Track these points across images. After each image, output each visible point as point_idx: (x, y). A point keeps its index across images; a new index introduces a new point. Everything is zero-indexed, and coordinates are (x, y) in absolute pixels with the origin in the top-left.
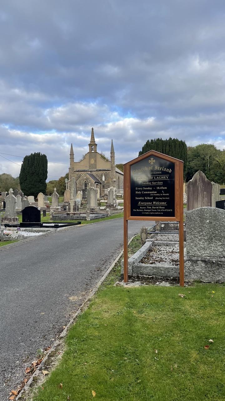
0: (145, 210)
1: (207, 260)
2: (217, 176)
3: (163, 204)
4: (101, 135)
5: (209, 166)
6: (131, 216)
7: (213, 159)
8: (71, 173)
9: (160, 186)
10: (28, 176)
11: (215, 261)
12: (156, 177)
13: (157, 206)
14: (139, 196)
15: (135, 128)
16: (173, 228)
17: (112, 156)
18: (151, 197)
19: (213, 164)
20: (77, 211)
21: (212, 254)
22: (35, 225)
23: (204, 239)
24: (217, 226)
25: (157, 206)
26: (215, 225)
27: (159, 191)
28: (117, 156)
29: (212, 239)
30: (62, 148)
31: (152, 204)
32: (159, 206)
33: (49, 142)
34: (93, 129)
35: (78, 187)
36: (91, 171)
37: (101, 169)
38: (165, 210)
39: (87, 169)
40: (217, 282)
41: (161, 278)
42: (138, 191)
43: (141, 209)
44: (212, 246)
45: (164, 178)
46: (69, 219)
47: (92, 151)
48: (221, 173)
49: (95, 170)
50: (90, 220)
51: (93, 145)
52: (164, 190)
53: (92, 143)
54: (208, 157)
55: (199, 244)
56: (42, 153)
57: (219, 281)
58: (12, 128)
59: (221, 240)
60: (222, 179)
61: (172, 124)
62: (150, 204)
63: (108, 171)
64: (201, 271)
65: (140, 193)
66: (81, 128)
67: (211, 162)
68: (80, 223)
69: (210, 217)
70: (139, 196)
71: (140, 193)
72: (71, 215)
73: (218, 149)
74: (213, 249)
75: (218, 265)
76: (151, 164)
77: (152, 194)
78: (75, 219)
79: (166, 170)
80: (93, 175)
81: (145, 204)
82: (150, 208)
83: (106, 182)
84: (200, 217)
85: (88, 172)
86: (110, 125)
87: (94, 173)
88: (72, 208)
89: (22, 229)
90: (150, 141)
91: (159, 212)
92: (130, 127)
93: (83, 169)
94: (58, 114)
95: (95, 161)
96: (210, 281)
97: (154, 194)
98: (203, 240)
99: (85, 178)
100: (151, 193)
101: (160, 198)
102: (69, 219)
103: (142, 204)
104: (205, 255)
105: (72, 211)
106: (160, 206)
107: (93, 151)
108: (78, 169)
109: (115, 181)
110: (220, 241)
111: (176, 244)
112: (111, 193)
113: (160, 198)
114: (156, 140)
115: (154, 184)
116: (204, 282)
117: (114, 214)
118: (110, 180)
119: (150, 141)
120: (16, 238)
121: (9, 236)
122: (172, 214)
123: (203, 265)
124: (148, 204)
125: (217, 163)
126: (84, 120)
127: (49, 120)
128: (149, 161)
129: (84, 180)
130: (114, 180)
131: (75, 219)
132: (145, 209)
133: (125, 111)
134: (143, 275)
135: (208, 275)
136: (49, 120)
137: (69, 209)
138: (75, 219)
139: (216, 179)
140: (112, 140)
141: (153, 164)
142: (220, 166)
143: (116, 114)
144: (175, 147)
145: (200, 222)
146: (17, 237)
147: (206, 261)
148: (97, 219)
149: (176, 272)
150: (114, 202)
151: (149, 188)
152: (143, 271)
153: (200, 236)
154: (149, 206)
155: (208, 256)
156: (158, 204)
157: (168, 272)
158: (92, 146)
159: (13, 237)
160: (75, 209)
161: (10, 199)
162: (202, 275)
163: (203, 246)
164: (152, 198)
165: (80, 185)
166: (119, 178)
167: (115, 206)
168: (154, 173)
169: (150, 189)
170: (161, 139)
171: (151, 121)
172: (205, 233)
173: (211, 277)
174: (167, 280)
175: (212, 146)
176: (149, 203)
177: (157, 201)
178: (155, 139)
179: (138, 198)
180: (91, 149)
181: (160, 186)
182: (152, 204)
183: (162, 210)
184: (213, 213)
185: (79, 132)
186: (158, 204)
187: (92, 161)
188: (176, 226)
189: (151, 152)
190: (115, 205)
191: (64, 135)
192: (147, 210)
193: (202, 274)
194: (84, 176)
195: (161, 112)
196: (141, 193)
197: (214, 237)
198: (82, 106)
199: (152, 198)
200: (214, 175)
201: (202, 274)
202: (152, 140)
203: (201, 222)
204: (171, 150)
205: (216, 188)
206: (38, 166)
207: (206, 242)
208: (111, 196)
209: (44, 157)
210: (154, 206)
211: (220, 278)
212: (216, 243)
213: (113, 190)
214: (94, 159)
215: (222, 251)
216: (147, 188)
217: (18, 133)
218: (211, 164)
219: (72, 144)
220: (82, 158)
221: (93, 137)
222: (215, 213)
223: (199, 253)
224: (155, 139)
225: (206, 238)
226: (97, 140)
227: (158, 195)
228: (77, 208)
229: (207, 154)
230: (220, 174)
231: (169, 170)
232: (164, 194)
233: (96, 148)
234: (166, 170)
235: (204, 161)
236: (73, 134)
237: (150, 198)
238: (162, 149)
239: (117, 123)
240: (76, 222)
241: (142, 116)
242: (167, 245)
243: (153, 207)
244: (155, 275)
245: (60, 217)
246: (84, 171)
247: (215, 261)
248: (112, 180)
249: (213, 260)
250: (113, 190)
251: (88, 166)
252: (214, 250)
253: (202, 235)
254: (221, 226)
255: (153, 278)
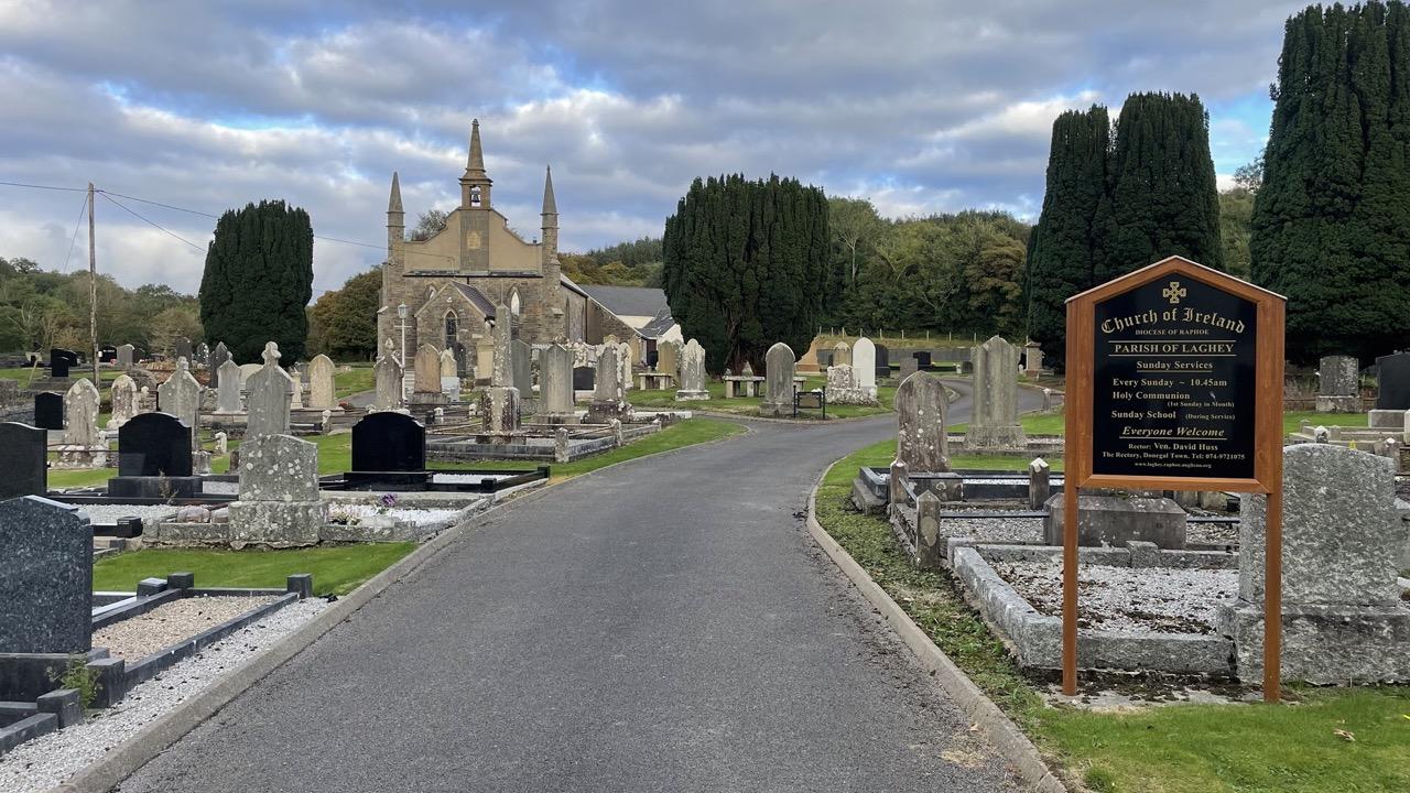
0: (1146, 455)
1: (1323, 614)
2: (882, 307)
3: (1214, 437)
4: (501, 149)
5: (857, 273)
6: (1095, 472)
7: (869, 249)
8: (391, 279)
9: (1202, 377)
10: (235, 289)
11: (1351, 617)
12: (1189, 346)
13: (1193, 442)
14: (1124, 406)
15: (612, 126)
16: (944, 495)
17: (549, 228)
18: (1170, 410)
19: (870, 266)
20: (515, 426)
21: (1336, 594)
22: (375, 482)
23: (1310, 547)
24: (1352, 507)
25: (1193, 442)
26: (1345, 502)
27: (1200, 394)
28: (563, 224)
29: (1335, 547)
30: (332, 183)
31: (1174, 434)
32: (1197, 442)
33: (287, 159)
34: (476, 125)
35: (422, 334)
36: (468, 277)
37: (508, 269)
38: (1221, 456)
39: (452, 268)
40: (1357, 682)
41: (1172, 677)
42: (1123, 389)
43: (1133, 451)
44: (1334, 570)
45: (1216, 348)
46: (486, 456)
47: (473, 204)
48: (894, 298)
49: (485, 273)
50: (567, 459)
51: (475, 181)
52: (1216, 389)
53: (473, 176)
54: (851, 243)
55: (1292, 562)
56: (293, 203)
57: (1359, 679)
58: (137, 99)
59: (1364, 549)
60: (897, 316)
61: (734, 125)
62: (1166, 436)
63: (534, 280)
64: (1305, 649)
65: (1127, 396)
66: (413, 114)
67: (862, 258)
68: (545, 473)
69: (1329, 476)
70: (1124, 406)
71: (1127, 396)
72: (494, 441)
73: (883, 215)
74: (1337, 578)
75: (1360, 629)
76: (1172, 302)
77: (1175, 401)
78: (513, 458)
79: (1134, 320)
80: (475, 290)
81: (1147, 433)
82: (1166, 447)
83: (525, 316)
84: (1298, 477)
85: (458, 280)
86: (525, 110)
87: (479, 284)
88: (497, 416)
89: (354, 495)
90: (705, 183)
91: (1196, 461)
92: (590, 121)
93: (422, 268)
94: (330, 57)
95: (486, 240)
96: (1331, 682)
97: (1179, 401)
98: (1307, 552)
99: (449, 300)
100: (1168, 397)
101: (1203, 417)
102: (486, 456)
103: (1135, 435)
104: (1312, 598)
105: (497, 429)
106: (1203, 442)
107: (478, 204)
108: (418, 268)
109: (557, 316)
110: (1360, 552)
111: (1052, 553)
112: (607, 361)
113: (1203, 417)
114: (725, 180)
115: (1180, 369)
116: (1314, 686)
117: (631, 437)
118: (539, 310)
119: (705, 183)
120: (387, 532)
121: (348, 527)
122: (1245, 469)
123: (1312, 630)
124: (1158, 436)
125: (883, 262)
126: (431, 88)
127: (295, 76)
128: (1185, 295)
129: (444, 309)
130: (556, 310)
131: (509, 458)
132: (1145, 450)
133: (583, 69)
134: (1104, 668)
135: (1327, 661)
136: (295, 76)
137: (488, 421)
138: (513, 458)
139: (879, 316)
140: (549, 169)
141: (1164, 296)
142: (891, 272)
143: (550, 70)
144: (793, 207)
145: (1298, 492)
146: (391, 529)
147: (1322, 619)
148: (585, 456)
149: (1218, 657)
150: (620, 395)
151: (1161, 383)
152: (1104, 656)
153: (1296, 538)
154: (1163, 442)
155: (1323, 603)
156: (1195, 436)
157: (1191, 658)
158: (475, 186)
159: (372, 530)
160: (507, 421)
161: (267, 383)
162: (1308, 662)
163: (1305, 570)
164: (1173, 415)
165: (429, 325)
166: (568, 304)
167: (624, 409)
168: (1182, 332)
169: (1167, 384)
170: (742, 176)
171: (667, 106)
172: (1314, 527)
173: (1337, 669)
174: (1195, 683)
175: (863, 207)
176: (1163, 432)
177: (1191, 424)
178: (722, 177)
179: (1120, 415)
180: (469, 198)
181: (1202, 377)
182: (1174, 434)
183: (1207, 456)
184: (1339, 463)
185: (407, 131)
186: (1195, 436)
187: (474, 241)
188: (956, 486)
189: (1174, 263)
190: (622, 405)
191: (346, 138)
192: (1154, 456)
193: (1306, 659)
194: (439, 292)
195: (703, 84)
196: (1134, 396)
197: (1341, 540)
198: (427, 36)
199: (1173, 415)
200: (872, 305)
201: (1306, 659)
202: (711, 180)
203: (1301, 492)
204: (780, 219)
205: (1009, 356)
206: (279, 251)
207: (1315, 556)
208: (607, 372)
209: (302, 217)
210: (1180, 442)
211: (1363, 671)
212: (1349, 559)
213: (614, 352)
214: (481, 233)
215: (1367, 586)
216: (1155, 383)
217: (161, 118)
218: (861, 265)
219: (396, 174)
220: (417, 224)
221: (476, 153)
222: (1346, 466)
223: (1295, 591)
224: (722, 177)
225: (1316, 544)
226: (490, 162)
227: (1194, 404)
228: (515, 415)
229: (849, 233)
230: (890, 302)
231: (1237, 323)
232: (1215, 404)
233: (486, 194)
234: (1134, 320)
235: (840, 256)
236: (381, 137)
237: (1165, 416)
238: (748, 214)
239: (550, 104)
240: (533, 466)
241: (641, 90)
242: (1024, 559)
243: (1176, 446)
244: (1146, 666)
245: (452, 449)
246: (442, 275)
247: (1351, 617)
248: (547, 313)
249: (1343, 614)
250: (614, 352)
251: (458, 259)
252: (1341, 581)
253: (1304, 534)
254: (1365, 506)
255: (1142, 677)
